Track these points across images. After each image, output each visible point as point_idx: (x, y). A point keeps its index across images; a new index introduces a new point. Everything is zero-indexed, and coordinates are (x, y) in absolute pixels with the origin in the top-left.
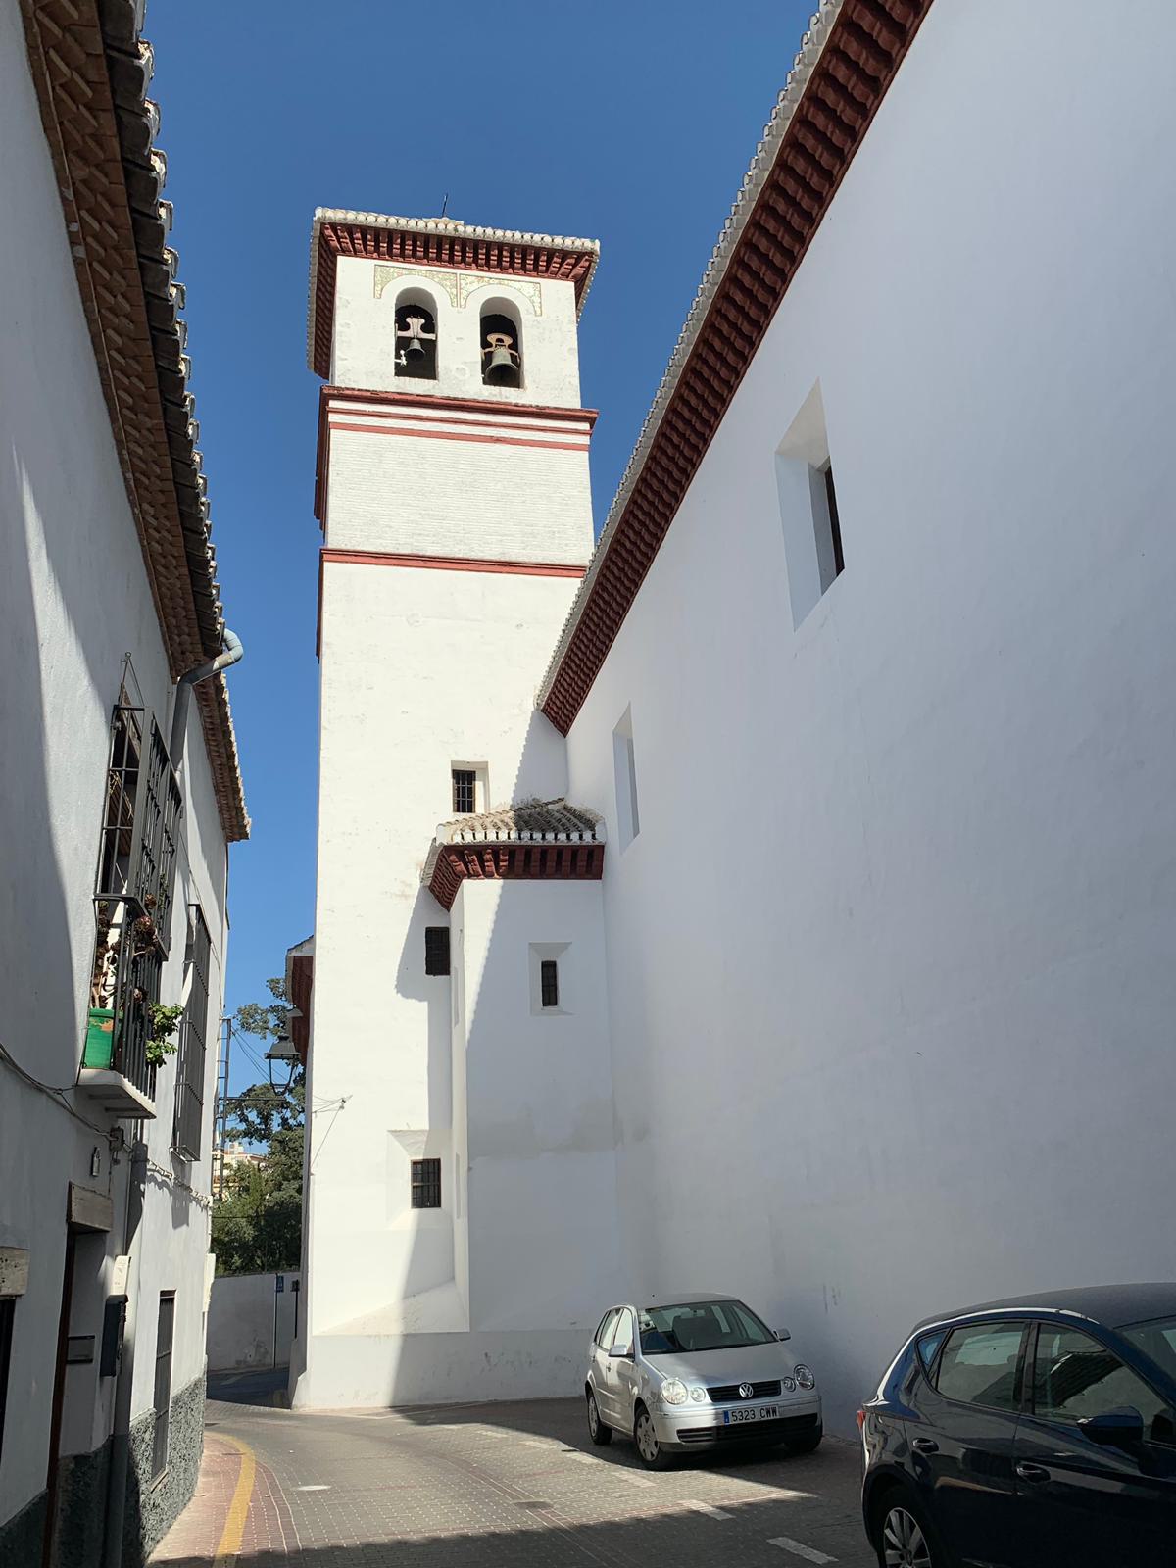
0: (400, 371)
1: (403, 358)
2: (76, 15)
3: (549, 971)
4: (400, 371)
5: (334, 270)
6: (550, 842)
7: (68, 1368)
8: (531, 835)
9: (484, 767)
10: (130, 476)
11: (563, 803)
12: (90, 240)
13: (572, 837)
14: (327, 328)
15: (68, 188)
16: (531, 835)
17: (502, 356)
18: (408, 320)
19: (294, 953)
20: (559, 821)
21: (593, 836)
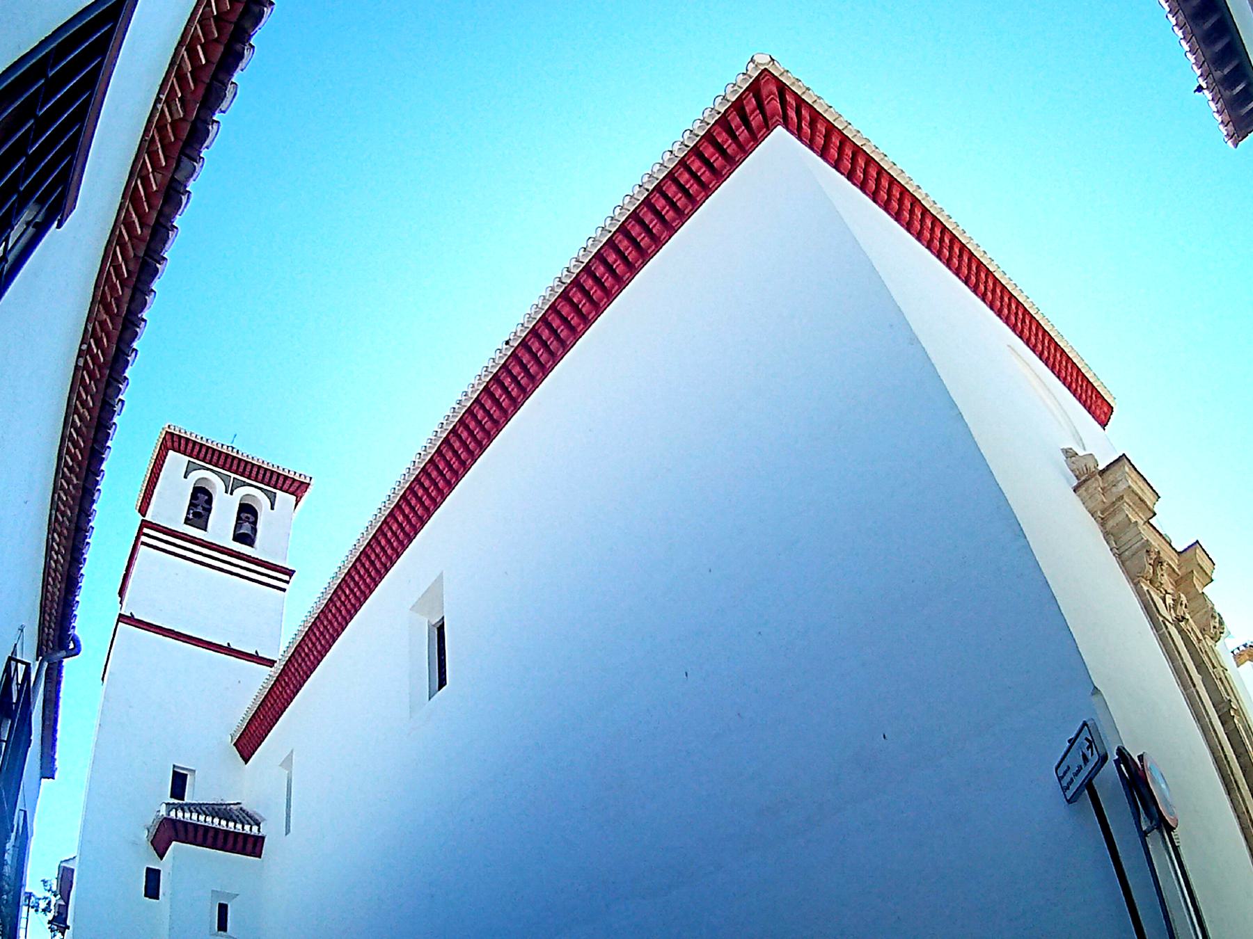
0: (187, 521)
1: (191, 515)
2: (139, 232)
3: (223, 909)
4: (187, 521)
10: (54, 512)
11: (240, 806)
12: (88, 357)
13: (245, 828)
15: (91, 323)
17: (246, 528)
20: (238, 816)
21: (259, 830)
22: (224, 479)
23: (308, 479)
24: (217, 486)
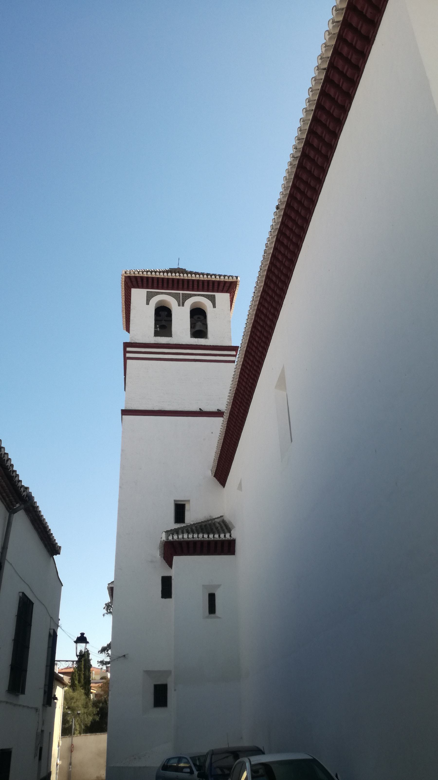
3: (212, 598)
4: (157, 334)
5: (130, 293)
6: (211, 538)
7: (129, 361)
8: (203, 536)
9: (175, 501)
14: (129, 297)
16: (203, 536)
17: (199, 327)
18: (160, 313)
19: (111, 586)
21: (230, 536)
22: (176, 297)
23: (235, 278)
24: (172, 303)
